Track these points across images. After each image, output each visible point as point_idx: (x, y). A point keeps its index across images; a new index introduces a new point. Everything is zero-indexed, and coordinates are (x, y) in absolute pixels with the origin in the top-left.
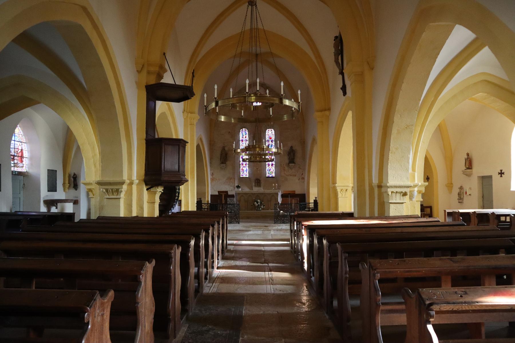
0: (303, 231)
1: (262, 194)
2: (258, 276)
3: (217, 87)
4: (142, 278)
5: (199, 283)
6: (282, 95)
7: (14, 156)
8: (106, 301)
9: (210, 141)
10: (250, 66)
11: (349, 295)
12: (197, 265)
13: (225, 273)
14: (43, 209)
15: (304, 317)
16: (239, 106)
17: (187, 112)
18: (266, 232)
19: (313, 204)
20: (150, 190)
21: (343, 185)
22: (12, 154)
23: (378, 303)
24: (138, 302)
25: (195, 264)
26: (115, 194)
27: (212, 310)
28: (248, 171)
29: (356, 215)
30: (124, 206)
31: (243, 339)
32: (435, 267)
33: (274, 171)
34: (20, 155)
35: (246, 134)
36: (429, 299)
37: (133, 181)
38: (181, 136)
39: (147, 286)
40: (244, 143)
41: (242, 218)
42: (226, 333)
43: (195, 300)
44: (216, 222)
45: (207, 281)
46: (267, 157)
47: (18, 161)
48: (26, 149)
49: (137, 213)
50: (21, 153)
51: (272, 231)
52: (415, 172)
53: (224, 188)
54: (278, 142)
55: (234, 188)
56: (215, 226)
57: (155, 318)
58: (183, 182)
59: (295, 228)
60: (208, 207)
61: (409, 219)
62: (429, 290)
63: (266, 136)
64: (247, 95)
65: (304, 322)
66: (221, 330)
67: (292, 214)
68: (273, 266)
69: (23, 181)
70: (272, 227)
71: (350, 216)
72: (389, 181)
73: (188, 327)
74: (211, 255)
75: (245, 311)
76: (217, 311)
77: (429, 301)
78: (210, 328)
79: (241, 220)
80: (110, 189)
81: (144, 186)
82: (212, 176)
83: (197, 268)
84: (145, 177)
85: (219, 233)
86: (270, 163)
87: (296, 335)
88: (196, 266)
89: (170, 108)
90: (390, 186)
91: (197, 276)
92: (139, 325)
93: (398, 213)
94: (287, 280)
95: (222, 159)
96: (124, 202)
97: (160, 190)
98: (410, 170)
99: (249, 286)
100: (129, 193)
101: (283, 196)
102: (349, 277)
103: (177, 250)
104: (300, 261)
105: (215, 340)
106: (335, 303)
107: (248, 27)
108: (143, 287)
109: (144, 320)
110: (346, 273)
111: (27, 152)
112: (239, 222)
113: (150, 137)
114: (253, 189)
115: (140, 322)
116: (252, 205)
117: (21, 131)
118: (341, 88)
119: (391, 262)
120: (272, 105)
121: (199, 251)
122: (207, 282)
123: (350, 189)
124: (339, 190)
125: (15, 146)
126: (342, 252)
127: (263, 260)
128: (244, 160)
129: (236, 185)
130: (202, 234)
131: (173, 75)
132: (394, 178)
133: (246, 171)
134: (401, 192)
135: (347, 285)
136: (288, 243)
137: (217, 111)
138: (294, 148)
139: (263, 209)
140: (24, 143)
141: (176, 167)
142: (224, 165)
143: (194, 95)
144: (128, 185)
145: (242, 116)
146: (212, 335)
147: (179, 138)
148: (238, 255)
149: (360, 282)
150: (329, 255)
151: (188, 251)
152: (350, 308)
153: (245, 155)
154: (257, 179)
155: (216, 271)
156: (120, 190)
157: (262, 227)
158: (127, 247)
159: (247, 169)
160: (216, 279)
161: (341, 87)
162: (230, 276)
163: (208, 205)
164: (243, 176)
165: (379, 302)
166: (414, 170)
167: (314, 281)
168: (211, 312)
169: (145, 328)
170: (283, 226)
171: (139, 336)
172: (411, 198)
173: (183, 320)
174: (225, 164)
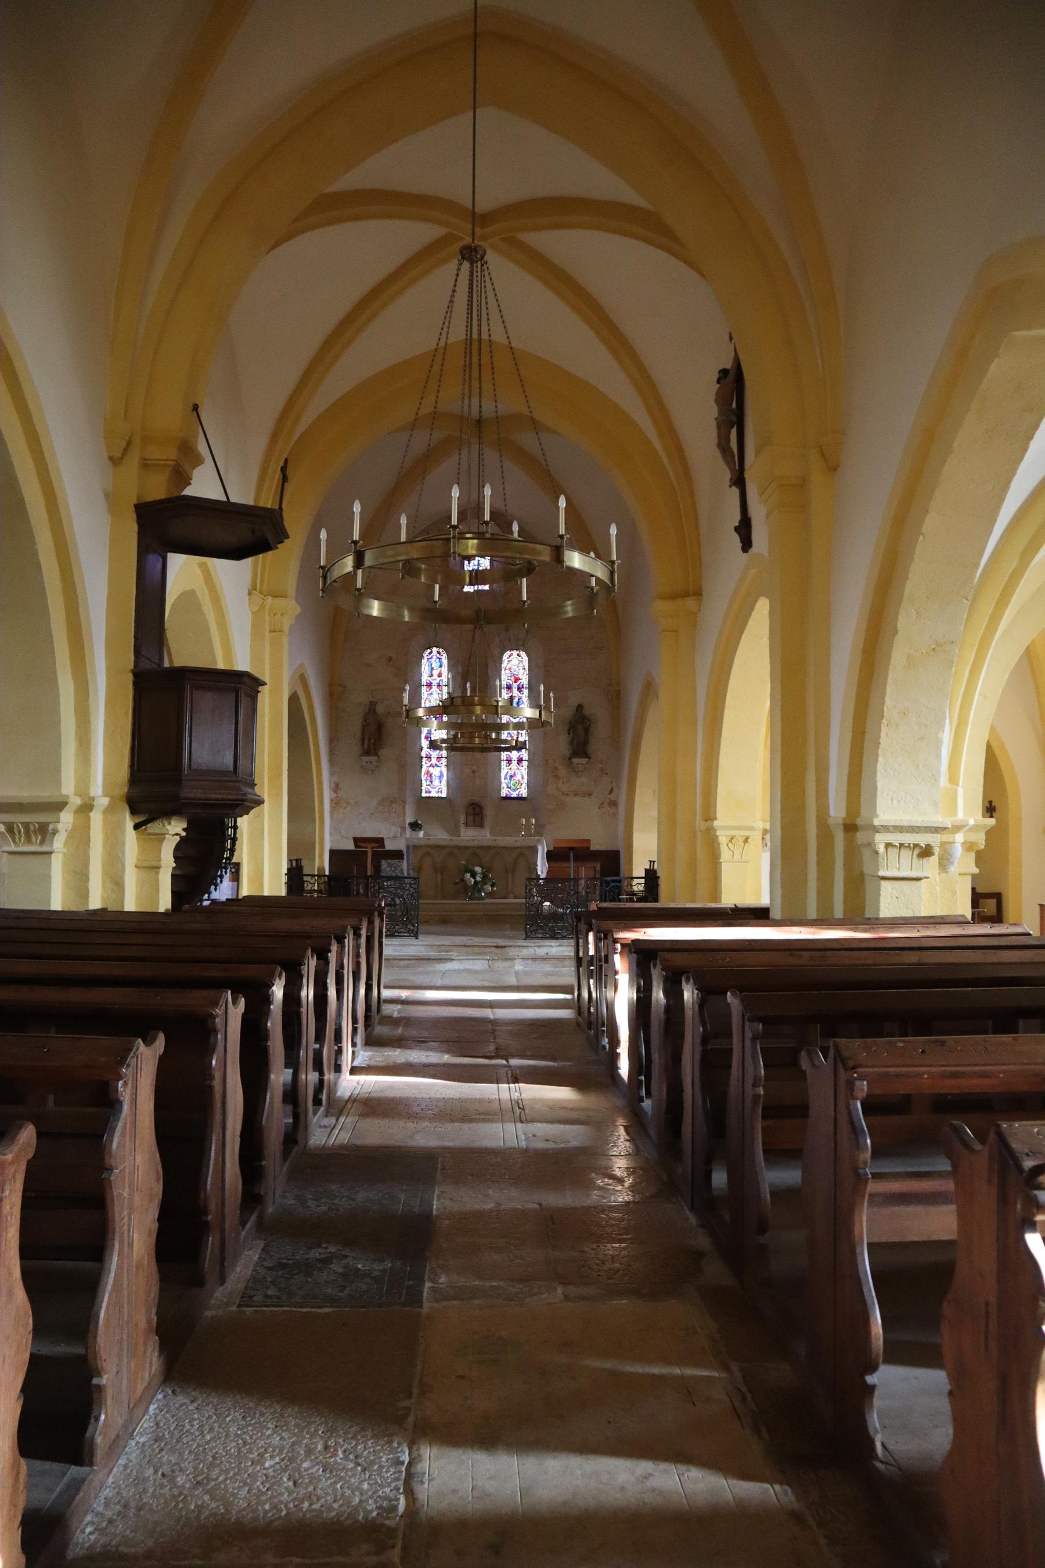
0: (617, 958)
1: (489, 848)
2: (478, 1097)
3: (359, 509)
4: (124, 1090)
5: (296, 1116)
6: (561, 537)
8: (9, 1157)
9: (331, 685)
10: (465, 453)
11: (764, 1151)
12: (292, 1061)
13: (376, 1085)
15: (621, 1220)
16: (426, 569)
17: (261, 592)
18: (500, 965)
19: (643, 881)
20: (146, 829)
21: (737, 824)
23: (861, 1171)
24: (111, 1166)
25: (286, 1054)
26: (37, 839)
27: (337, 1197)
28: (445, 778)
29: (776, 914)
30: (64, 877)
31: (436, 1285)
32: (1036, 1064)
33: (526, 781)
35: (441, 666)
36: (1030, 1154)
37: (93, 799)
38: (242, 664)
39: (137, 1117)
40: (434, 693)
41: (426, 922)
42: (380, 1268)
43: (285, 1168)
44: (349, 927)
45: (322, 1109)
46: (504, 735)
49: (103, 899)
51: (517, 962)
52: (958, 785)
53: (370, 829)
54: (542, 688)
55: (403, 829)
56: (346, 940)
57: (161, 1218)
58: (249, 804)
59: (592, 952)
60: (322, 886)
61: (938, 926)
62: (1032, 1125)
63: (503, 672)
64: (454, 534)
65: (622, 1235)
66: (367, 1260)
67: (580, 910)
68: (521, 1068)
70: (517, 949)
71: (759, 915)
72: (879, 811)
73: (263, 1250)
74: (333, 1027)
75: (438, 1200)
76: (353, 1200)
77: (1033, 1160)
78: (330, 1253)
79: (423, 928)
80: (22, 823)
81: (128, 815)
83: (291, 1071)
84: (129, 789)
85: (358, 965)
86: (514, 755)
87: (599, 1276)
88: (287, 1065)
89: (207, 574)
90: (882, 826)
91: (292, 1095)
92: (113, 1239)
93: (905, 910)
94: (565, 1108)
95: (366, 741)
96: (65, 865)
97: (176, 828)
98: (944, 781)
99: (449, 1126)
100: (81, 838)
101: (551, 856)
102: (764, 1094)
103: (233, 1009)
104: (605, 1053)
105: (348, 1289)
106: (719, 1178)
107: (458, 333)
108: (126, 1119)
109: (129, 1225)
110: (755, 1085)
112: (417, 933)
113: (146, 665)
114: (462, 834)
115: (117, 1230)
116: (456, 883)
118: (737, 529)
119: (900, 1045)
120: (529, 569)
121: (299, 1015)
122: (319, 1114)
123: (756, 837)
124: (723, 840)
126: (746, 1018)
127: (492, 1047)
128: (433, 745)
129: (409, 819)
130: (306, 962)
131: (221, 473)
132: (895, 802)
133: (441, 776)
134: (916, 846)
135: (760, 1119)
136: (569, 997)
137: (359, 585)
138: (587, 711)
139: (490, 895)
141: (228, 760)
142: (373, 758)
143: (287, 537)
144: (76, 812)
145: (435, 602)
146: (338, 1273)
147: (235, 669)
148: (413, 1032)
149: (801, 1110)
150: (701, 1029)
151: (266, 1013)
152: (768, 1191)
153: (440, 728)
154: (472, 804)
155: (347, 1081)
156: (51, 827)
157: (487, 950)
158: (76, 996)
160: (349, 1105)
161: (737, 524)
162: (391, 1094)
163: (323, 880)
164: (430, 792)
165: (864, 1169)
166: (953, 779)
167: (650, 1113)
168: (333, 1204)
169: (132, 1250)
170: (551, 946)
171: (112, 1274)
172: (944, 864)
173: (248, 1226)
174: (376, 755)
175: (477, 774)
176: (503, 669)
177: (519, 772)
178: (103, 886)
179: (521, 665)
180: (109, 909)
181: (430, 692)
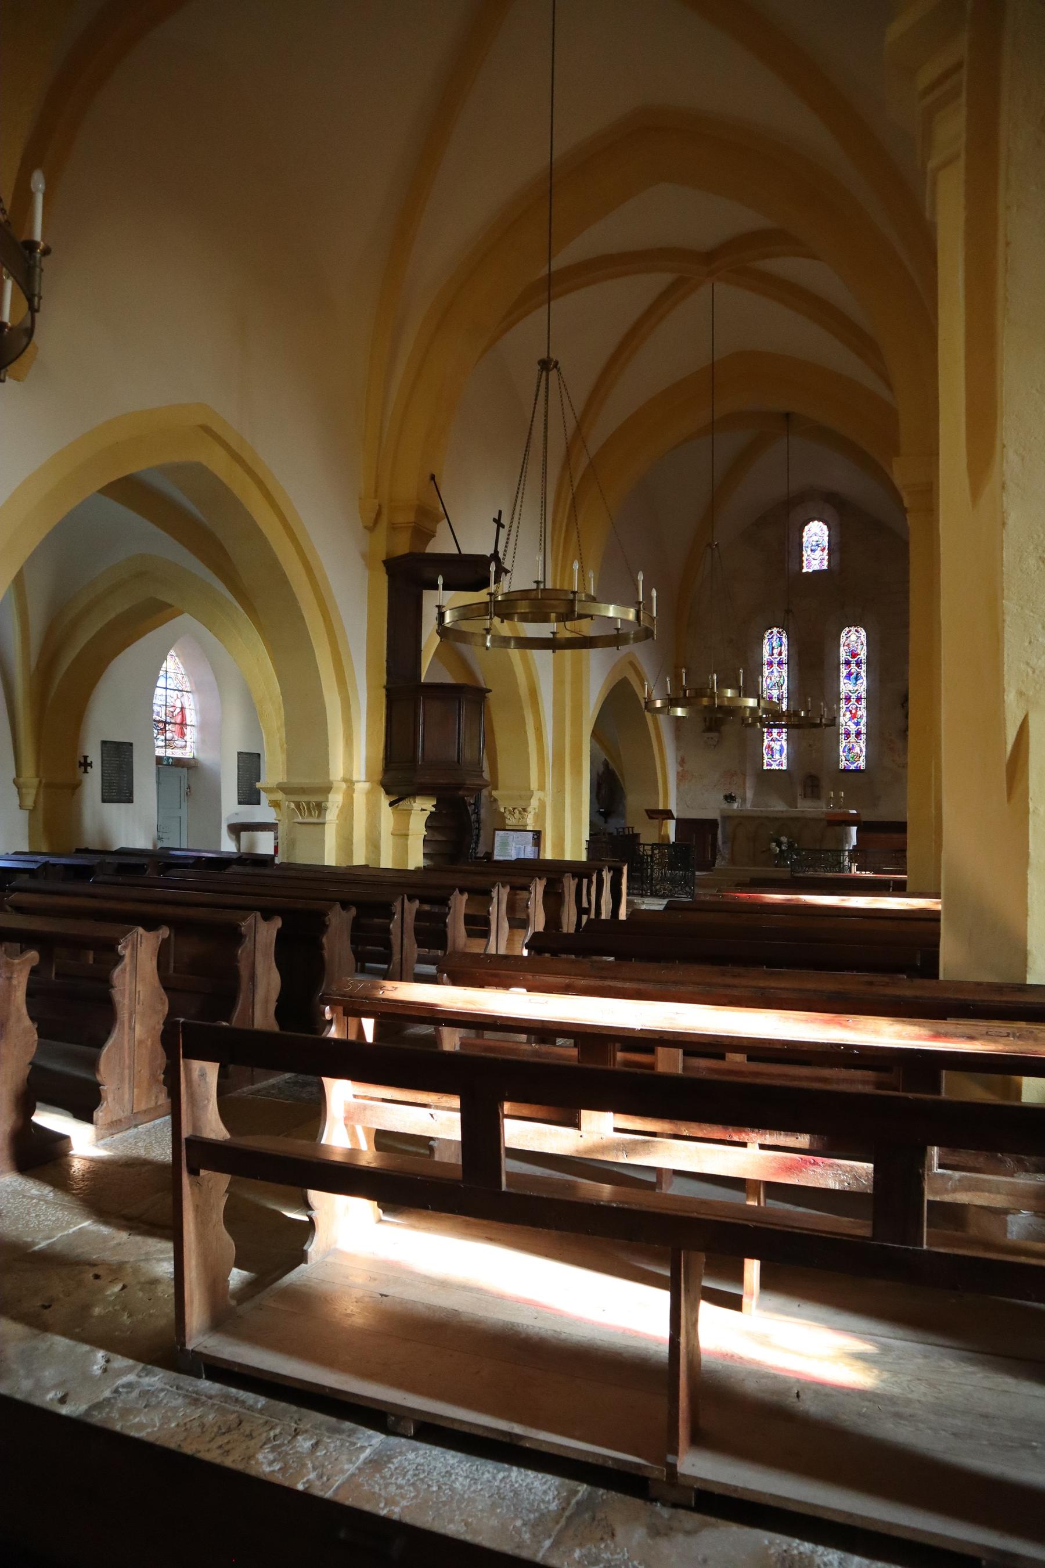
7: (165, 723)
14: (228, 846)
22: (161, 719)
28: (785, 752)
33: (864, 754)
34: (179, 720)
40: (775, 671)
47: (174, 734)
48: (192, 707)
50: (180, 717)
63: (842, 648)
69: (186, 781)
82: (681, 766)
97: (422, 808)
111: (193, 712)
117: (180, 666)
125: (168, 701)
133: (781, 751)
140: (187, 692)
142: (715, 735)
159: (782, 746)
164: (771, 765)
174: (718, 731)
176: (842, 645)
178: (367, 849)
180: (370, 866)
181: (771, 670)
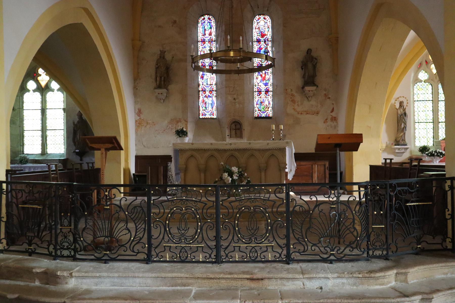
9: (133, 40)
33: (271, 106)
35: (211, 28)
40: (207, 46)
63: (254, 30)
70: (279, 282)
95: (158, 79)
138: (314, 54)
142: (164, 91)
154: (234, 122)
164: (205, 115)
175: (237, 101)
177: (267, 100)
179: (266, 25)
